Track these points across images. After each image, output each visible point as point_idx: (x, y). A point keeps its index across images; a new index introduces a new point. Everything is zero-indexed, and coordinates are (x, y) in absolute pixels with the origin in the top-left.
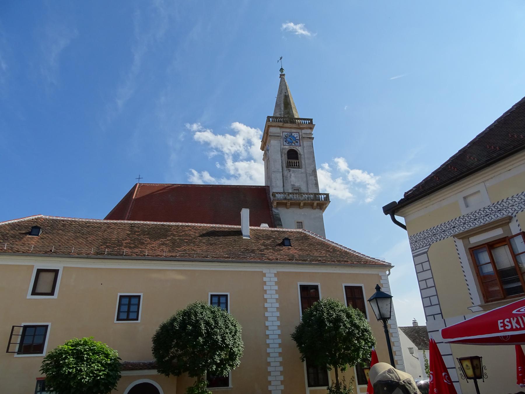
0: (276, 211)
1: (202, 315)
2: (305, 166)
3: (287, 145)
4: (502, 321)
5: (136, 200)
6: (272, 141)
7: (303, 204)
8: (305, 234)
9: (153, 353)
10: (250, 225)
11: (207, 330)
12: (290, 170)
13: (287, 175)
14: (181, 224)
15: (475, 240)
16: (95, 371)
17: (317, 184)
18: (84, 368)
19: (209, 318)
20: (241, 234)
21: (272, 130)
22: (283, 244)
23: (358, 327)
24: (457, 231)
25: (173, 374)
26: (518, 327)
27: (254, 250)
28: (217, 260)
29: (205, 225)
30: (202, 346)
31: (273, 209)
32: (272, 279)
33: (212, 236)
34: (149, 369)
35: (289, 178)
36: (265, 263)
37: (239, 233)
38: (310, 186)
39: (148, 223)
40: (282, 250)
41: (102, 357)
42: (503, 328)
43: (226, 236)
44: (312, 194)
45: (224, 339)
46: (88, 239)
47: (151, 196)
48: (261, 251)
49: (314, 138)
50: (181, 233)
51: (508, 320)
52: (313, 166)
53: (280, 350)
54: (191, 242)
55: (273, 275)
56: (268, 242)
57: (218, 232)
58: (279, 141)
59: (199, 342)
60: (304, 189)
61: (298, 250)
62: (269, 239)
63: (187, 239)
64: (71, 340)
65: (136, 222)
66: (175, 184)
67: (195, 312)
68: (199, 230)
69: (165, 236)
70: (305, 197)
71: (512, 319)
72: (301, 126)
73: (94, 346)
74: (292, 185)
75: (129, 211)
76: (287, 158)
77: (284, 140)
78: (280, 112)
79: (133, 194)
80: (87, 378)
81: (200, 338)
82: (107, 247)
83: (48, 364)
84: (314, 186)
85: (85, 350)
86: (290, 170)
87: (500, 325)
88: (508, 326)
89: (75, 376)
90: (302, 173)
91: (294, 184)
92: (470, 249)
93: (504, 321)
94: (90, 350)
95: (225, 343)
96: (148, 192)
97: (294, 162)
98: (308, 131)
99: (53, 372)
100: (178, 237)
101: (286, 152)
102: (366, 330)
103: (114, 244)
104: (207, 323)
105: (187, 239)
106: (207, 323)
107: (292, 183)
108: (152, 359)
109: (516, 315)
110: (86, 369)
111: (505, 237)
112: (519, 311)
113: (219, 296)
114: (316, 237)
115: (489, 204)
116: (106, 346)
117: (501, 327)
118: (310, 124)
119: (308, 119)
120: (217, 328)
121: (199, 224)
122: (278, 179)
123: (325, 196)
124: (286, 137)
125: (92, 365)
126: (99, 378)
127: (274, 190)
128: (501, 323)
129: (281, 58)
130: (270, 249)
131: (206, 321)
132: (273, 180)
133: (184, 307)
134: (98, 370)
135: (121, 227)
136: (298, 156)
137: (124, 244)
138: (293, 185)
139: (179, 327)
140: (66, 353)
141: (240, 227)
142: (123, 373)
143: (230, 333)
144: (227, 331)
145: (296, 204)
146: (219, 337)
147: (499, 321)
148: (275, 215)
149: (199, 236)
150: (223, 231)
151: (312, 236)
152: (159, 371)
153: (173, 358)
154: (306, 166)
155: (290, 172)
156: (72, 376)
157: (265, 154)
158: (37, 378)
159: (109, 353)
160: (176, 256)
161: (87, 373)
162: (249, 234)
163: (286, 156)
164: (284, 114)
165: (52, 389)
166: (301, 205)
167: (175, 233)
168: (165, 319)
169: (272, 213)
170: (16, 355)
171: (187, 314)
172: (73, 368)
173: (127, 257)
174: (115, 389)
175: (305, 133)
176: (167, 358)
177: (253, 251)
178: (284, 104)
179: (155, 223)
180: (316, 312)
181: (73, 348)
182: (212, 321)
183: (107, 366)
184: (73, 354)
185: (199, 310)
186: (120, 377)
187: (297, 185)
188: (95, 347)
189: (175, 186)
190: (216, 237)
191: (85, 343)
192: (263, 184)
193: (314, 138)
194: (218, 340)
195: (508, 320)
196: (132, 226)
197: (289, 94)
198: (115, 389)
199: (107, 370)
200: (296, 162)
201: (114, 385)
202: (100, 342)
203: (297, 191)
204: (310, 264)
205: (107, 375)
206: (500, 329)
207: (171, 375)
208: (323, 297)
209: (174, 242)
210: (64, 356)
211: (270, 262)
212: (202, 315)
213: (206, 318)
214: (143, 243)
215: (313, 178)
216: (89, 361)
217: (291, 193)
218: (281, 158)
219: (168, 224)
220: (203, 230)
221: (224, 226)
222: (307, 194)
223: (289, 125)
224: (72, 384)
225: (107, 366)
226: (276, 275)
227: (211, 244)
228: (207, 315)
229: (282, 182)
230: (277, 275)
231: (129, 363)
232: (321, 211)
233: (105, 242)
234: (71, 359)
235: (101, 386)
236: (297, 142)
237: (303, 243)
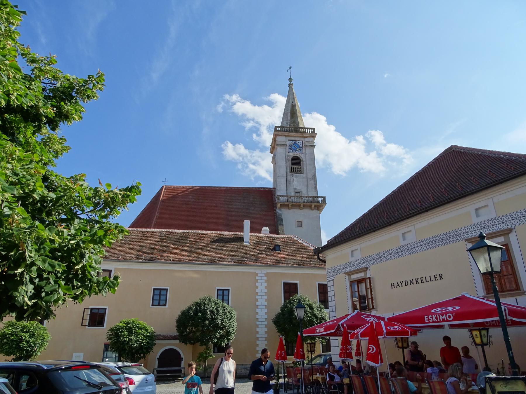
0: (280, 212)
1: (209, 306)
2: (307, 171)
3: (292, 152)
4: (427, 316)
5: (162, 201)
6: (278, 149)
7: (302, 206)
8: (294, 239)
9: (176, 330)
10: (250, 232)
11: (211, 316)
12: (293, 175)
13: (290, 180)
14: (197, 231)
15: (355, 277)
16: (140, 340)
17: (316, 188)
18: (133, 338)
19: (213, 308)
20: (243, 241)
21: (279, 139)
22: (274, 249)
23: (316, 316)
24: (347, 270)
25: (189, 343)
26: (436, 320)
27: (251, 254)
28: (223, 263)
29: (216, 232)
30: (208, 326)
31: (277, 210)
32: (263, 278)
33: (220, 242)
34: (174, 339)
35: (292, 182)
36: (258, 266)
37: (241, 239)
38: (310, 189)
39: (173, 230)
40: (272, 255)
41: (144, 331)
42: (428, 321)
43: (231, 242)
44: (311, 197)
45: (222, 322)
46: (130, 246)
47: (175, 197)
48: (256, 256)
49: (315, 146)
50: (197, 240)
51: (431, 316)
52: (313, 171)
53: (266, 329)
54: (205, 248)
55: (264, 275)
56: (263, 248)
57: (225, 238)
58: (284, 149)
59: (206, 324)
60: (304, 193)
61: (285, 255)
62: (264, 245)
63: (201, 246)
64: (124, 320)
65: (163, 231)
66: (196, 186)
67: (204, 303)
68: (211, 237)
69: (185, 243)
70: (305, 199)
71: (433, 316)
72: (305, 135)
73: (138, 324)
74: (294, 188)
75: (157, 211)
76: (291, 164)
77: (289, 148)
78: (287, 120)
79: (161, 196)
80: (136, 344)
81: (206, 321)
82: (144, 253)
83: (110, 335)
84: (313, 189)
85: (133, 327)
86: (293, 175)
87: (426, 319)
88: (431, 320)
89: (128, 342)
90: (303, 178)
91: (296, 187)
92: (351, 282)
93: (428, 317)
94: (136, 326)
95: (223, 325)
96: (173, 194)
97: (297, 168)
98: (311, 139)
99: (115, 340)
100: (194, 243)
101: (290, 159)
102: (323, 319)
103: (148, 250)
104: (212, 312)
105: (201, 246)
106: (212, 312)
107: (294, 187)
108: (176, 333)
109: (434, 314)
110: (134, 339)
111: (364, 278)
112: (435, 311)
113: (223, 290)
114: (303, 243)
115: (360, 258)
116: (146, 324)
117: (427, 320)
118: (313, 134)
119: (311, 129)
120: (219, 315)
121: (211, 232)
122: (282, 184)
123: (322, 199)
124: (291, 146)
125: (138, 336)
126: (142, 344)
127: (278, 193)
128: (426, 318)
129: (290, 68)
130: (264, 254)
131: (211, 310)
132: (278, 184)
133: (197, 300)
134: (142, 339)
135: (152, 235)
136: (300, 162)
137: (156, 251)
138: (295, 189)
139: (193, 314)
140: (122, 328)
141: (242, 233)
142: (157, 342)
143: (227, 319)
144: (225, 317)
145: (297, 206)
146: (219, 321)
147: (425, 317)
148: (278, 215)
149: (211, 243)
150: (229, 238)
151: (300, 241)
152: (180, 341)
153: (189, 333)
154: (308, 172)
155: (293, 176)
156: (126, 343)
157: (274, 158)
158: (104, 343)
159: (149, 329)
160: (192, 261)
161: (135, 341)
162: (249, 241)
163: (290, 162)
164: (290, 123)
165: (114, 350)
166: (301, 206)
167: (193, 240)
168: (185, 307)
169: (276, 214)
170: (87, 327)
171: (198, 305)
172: (127, 337)
173: (157, 261)
174: (152, 352)
175: (308, 141)
176: (186, 333)
177: (250, 256)
178: (291, 113)
179: (178, 231)
180: (290, 304)
181: (126, 325)
182: (215, 311)
183: (147, 337)
184: (126, 329)
185: (207, 302)
186: (155, 344)
187: (298, 188)
188: (139, 325)
189: (195, 188)
190: (224, 244)
191: (133, 322)
192: (272, 187)
193: (315, 146)
194: (219, 323)
195: (431, 316)
196: (161, 234)
197: (296, 103)
198: (152, 352)
199: (147, 340)
200: (299, 168)
201: (151, 349)
202: (142, 322)
203: (299, 194)
204: (292, 267)
205: (148, 343)
206: (426, 321)
207: (188, 344)
208: (301, 293)
209: (191, 248)
210: (121, 330)
211: (262, 265)
212: (209, 306)
213: (211, 308)
214: (169, 249)
215: (312, 182)
216: (136, 334)
217: (292, 196)
218: (285, 164)
219: (188, 232)
220: (214, 237)
221: (230, 233)
222: (306, 197)
223: (293, 134)
224: (126, 347)
225: (147, 337)
226: (266, 275)
227: (219, 250)
228: (212, 306)
229: (286, 185)
230: (266, 275)
231: (160, 335)
232: (319, 212)
233: (142, 248)
234: (126, 332)
235: (143, 349)
236: (300, 150)
237: (290, 248)
